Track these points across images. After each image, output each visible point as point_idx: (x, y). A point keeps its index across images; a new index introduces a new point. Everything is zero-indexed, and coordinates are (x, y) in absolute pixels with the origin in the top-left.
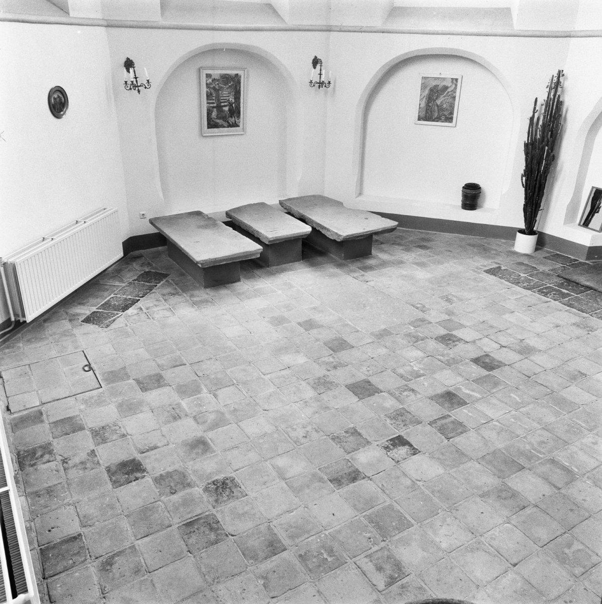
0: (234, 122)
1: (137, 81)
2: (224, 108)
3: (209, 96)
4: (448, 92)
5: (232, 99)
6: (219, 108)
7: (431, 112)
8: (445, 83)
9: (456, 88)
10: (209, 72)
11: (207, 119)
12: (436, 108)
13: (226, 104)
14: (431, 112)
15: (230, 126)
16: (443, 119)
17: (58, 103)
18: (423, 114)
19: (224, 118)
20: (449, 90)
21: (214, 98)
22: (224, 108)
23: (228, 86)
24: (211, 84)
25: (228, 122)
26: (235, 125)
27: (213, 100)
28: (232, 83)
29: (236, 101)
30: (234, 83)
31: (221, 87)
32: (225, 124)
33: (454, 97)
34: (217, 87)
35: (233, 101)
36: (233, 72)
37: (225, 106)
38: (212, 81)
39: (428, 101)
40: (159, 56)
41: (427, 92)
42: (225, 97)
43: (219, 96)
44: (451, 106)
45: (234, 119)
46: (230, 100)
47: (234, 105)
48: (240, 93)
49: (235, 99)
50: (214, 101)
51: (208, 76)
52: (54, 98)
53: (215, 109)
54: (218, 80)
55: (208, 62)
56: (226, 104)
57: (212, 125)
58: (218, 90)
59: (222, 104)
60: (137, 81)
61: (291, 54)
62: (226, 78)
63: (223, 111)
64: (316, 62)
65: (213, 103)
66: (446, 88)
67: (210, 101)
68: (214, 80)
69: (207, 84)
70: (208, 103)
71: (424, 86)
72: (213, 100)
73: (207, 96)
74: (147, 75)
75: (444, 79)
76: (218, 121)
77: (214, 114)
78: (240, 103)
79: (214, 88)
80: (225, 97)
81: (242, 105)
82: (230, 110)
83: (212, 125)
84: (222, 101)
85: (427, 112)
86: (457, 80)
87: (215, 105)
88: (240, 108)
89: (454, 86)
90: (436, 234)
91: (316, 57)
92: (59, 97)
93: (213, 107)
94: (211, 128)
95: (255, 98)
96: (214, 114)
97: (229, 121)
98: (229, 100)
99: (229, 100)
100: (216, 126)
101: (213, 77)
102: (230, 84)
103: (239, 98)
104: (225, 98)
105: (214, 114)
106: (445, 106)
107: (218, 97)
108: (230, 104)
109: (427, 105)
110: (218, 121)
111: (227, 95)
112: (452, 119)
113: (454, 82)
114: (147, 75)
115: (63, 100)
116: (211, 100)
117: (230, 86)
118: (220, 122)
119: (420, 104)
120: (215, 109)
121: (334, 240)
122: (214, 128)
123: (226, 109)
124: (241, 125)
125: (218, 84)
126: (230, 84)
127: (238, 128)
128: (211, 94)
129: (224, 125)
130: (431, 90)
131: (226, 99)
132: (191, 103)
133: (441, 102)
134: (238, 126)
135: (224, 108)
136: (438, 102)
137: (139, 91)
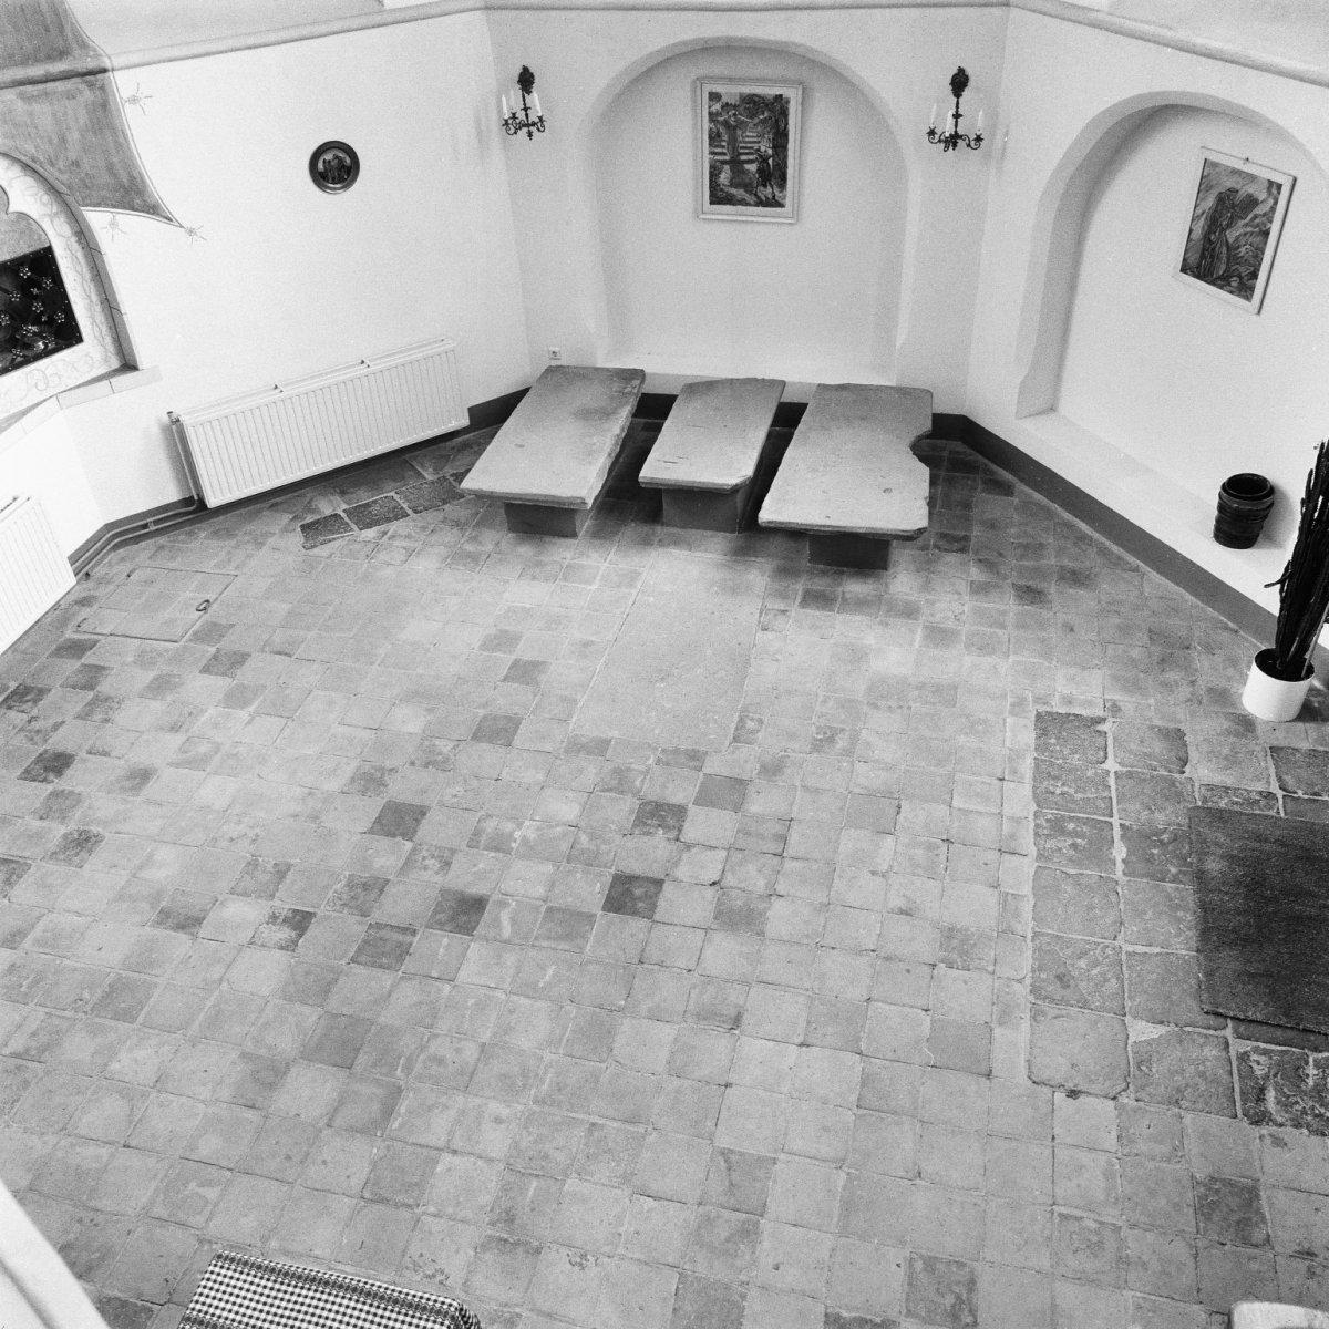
0: (770, 196)
1: (527, 115)
2: (751, 157)
3: (714, 138)
4: (1256, 217)
5: (766, 147)
6: (736, 164)
7: (1212, 257)
8: (1251, 189)
9: (1273, 209)
10: (717, 89)
11: (710, 184)
12: (1224, 249)
13: (751, 157)
14: (1212, 257)
15: (760, 203)
16: (1233, 284)
17: (335, 167)
18: (1193, 260)
19: (748, 187)
20: (1260, 210)
21: (724, 144)
22: (747, 167)
23: (756, 120)
24: (718, 114)
25: (756, 195)
26: (774, 203)
27: (723, 147)
28: (766, 115)
29: (776, 153)
30: (772, 114)
31: (743, 122)
32: (752, 199)
33: (1266, 234)
34: (732, 121)
35: (770, 151)
36: (770, 91)
37: (749, 162)
38: (722, 107)
39: (1209, 227)
40: (584, 60)
41: (1210, 202)
42: (750, 142)
43: (736, 140)
44: (1256, 256)
45: (769, 190)
46: (763, 149)
47: (770, 161)
48: (786, 136)
49: (774, 147)
50: (725, 150)
51: (714, 97)
52: (324, 161)
53: (727, 167)
54: (735, 107)
55: (720, 67)
56: (751, 157)
57: (718, 197)
58: (735, 128)
59: (743, 158)
60: (527, 115)
61: (896, 63)
62: (753, 103)
63: (745, 172)
64: (959, 82)
65: (724, 154)
66: (1252, 202)
67: (717, 150)
68: (726, 106)
69: (710, 114)
70: (712, 153)
71: (1205, 184)
72: (723, 147)
73: (710, 138)
74: (538, 108)
75: (1252, 178)
76: (733, 191)
77: (724, 177)
78: (786, 157)
79: (726, 124)
80: (750, 142)
81: (790, 161)
82: (760, 171)
83: (718, 197)
84: (742, 151)
85: (1203, 256)
86: (1279, 187)
87: (727, 158)
88: (786, 166)
89: (1271, 201)
90: (1136, 569)
91: (961, 71)
92: (336, 157)
93: (723, 162)
94: (719, 203)
95: (819, 149)
96: (724, 177)
97: (759, 194)
98: (758, 150)
99: (758, 150)
100: (729, 200)
101: (725, 99)
102: (761, 117)
103: (785, 148)
104: (749, 145)
105: (725, 177)
106: (1243, 250)
107: (733, 141)
108: (763, 159)
109: (1206, 237)
110: (733, 191)
111: (756, 139)
112: (1253, 291)
113: (1274, 191)
114: (538, 108)
115: (348, 160)
116: (717, 146)
117: (762, 121)
118: (739, 193)
119: (1191, 231)
120: (727, 167)
121: (928, 504)
122: (725, 204)
123: (752, 168)
124: (788, 202)
125: (735, 115)
126: (761, 117)
127: (779, 209)
128: (719, 135)
129: (748, 200)
130: (1221, 199)
131: (752, 148)
132: (677, 147)
133: (1237, 239)
134: (781, 205)
135: (751, 157)
136: (1231, 235)
137: (530, 135)
